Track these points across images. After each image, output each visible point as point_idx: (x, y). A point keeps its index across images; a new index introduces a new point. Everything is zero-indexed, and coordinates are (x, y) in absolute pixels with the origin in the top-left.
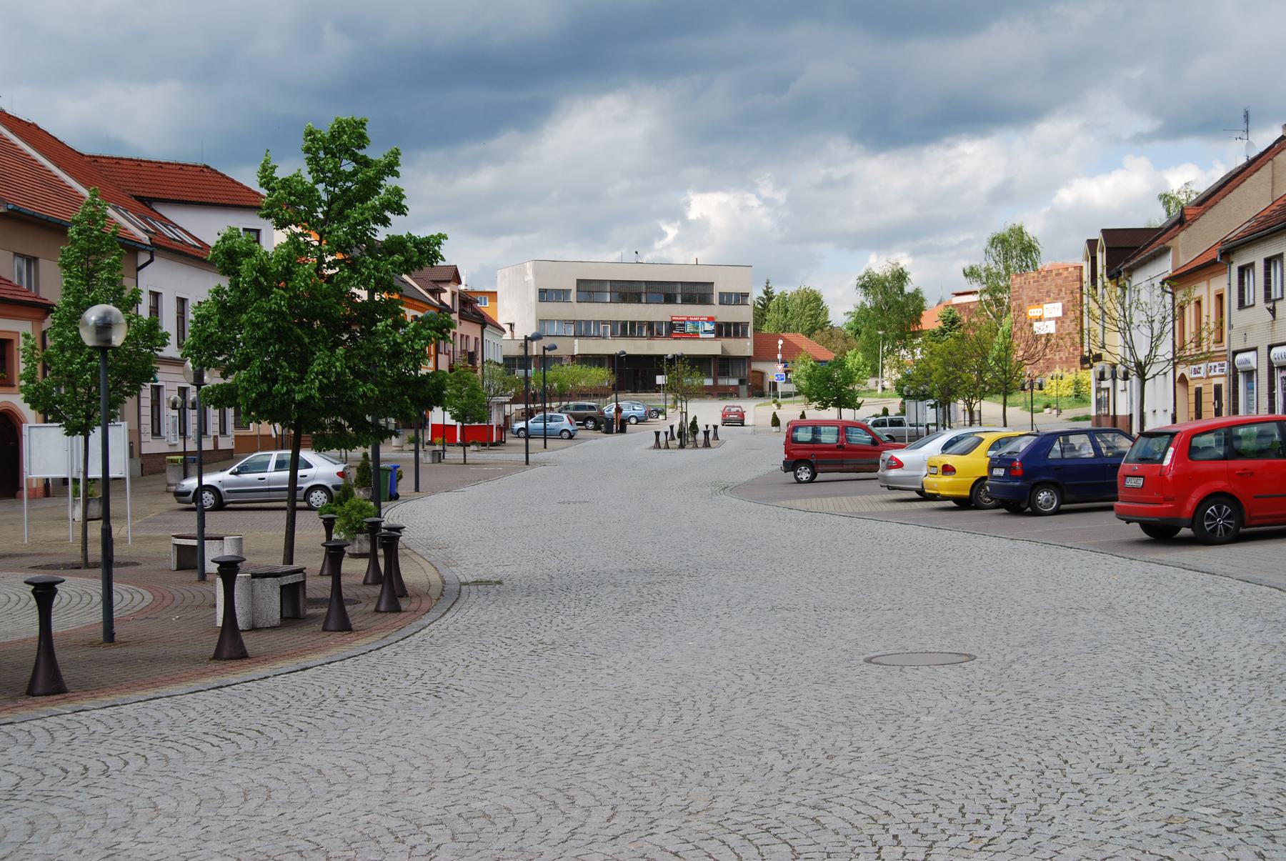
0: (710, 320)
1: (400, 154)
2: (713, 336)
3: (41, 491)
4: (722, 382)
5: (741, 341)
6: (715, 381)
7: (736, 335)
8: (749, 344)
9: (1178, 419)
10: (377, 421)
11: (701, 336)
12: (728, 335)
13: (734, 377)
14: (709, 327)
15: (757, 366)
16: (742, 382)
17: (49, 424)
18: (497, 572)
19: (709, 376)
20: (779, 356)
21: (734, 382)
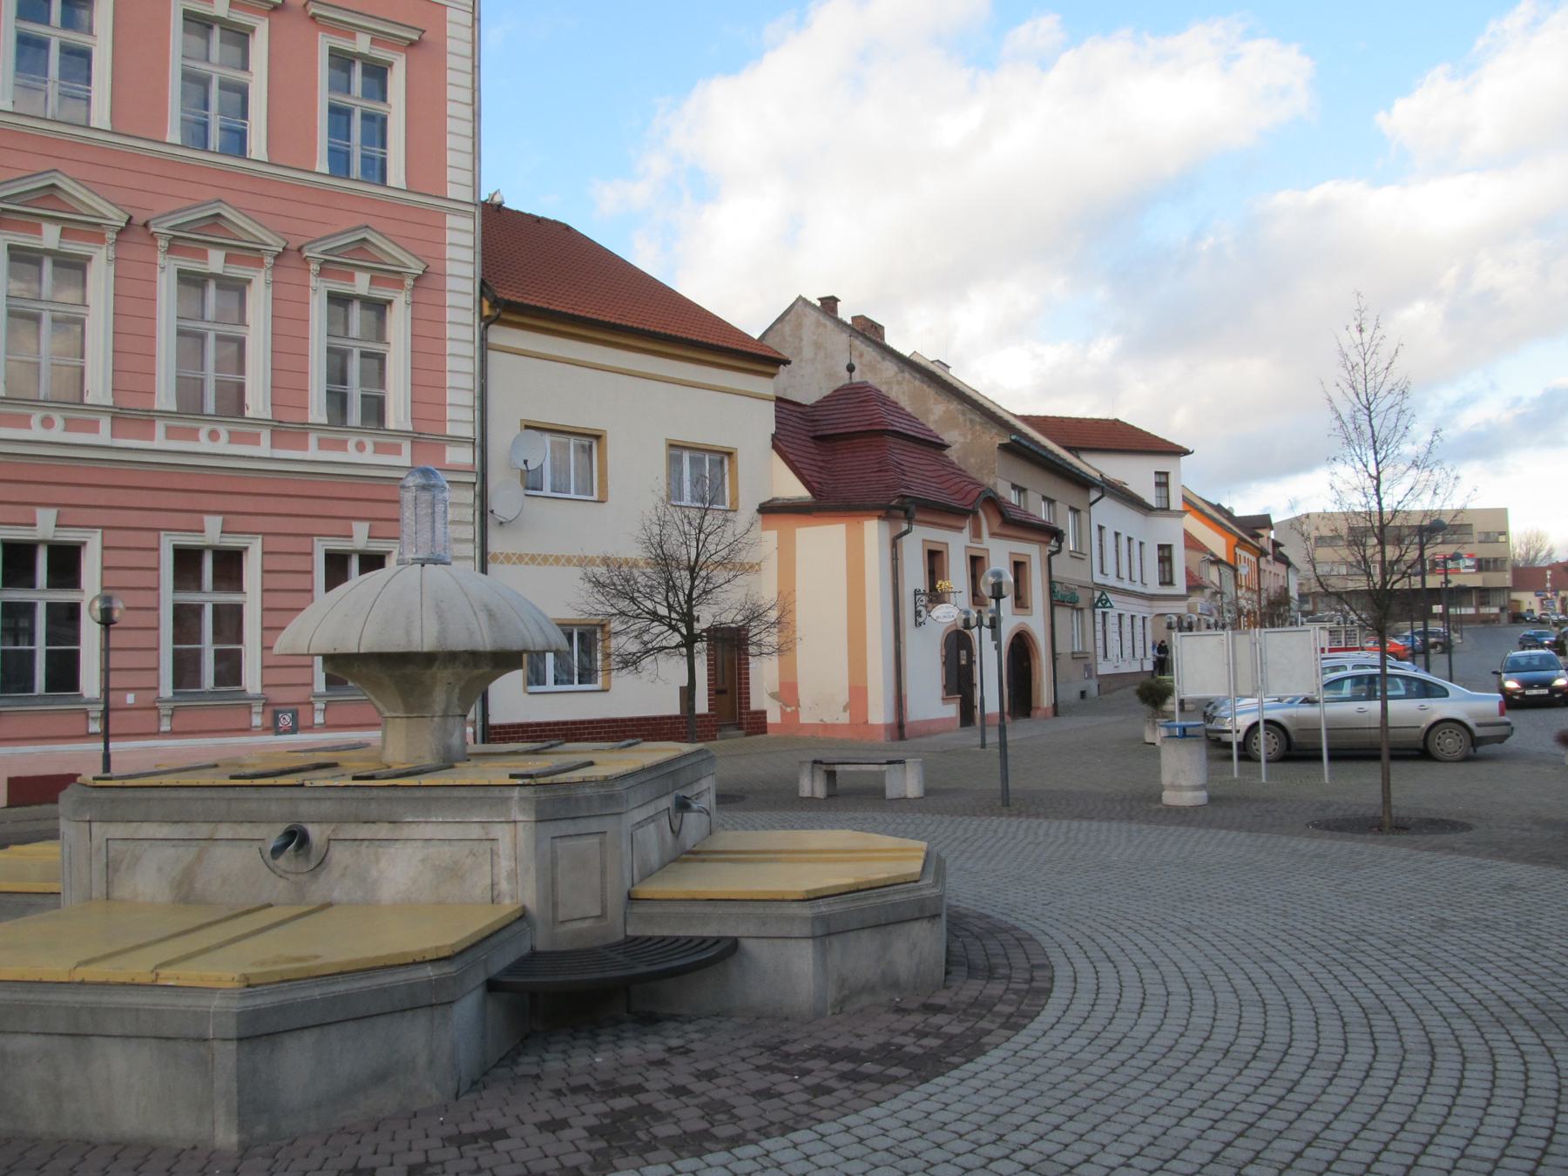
0: (1470, 556)
1: (829, 304)
2: (1474, 570)
3: (1051, 711)
4: (1484, 610)
5: (1499, 575)
6: (1477, 610)
7: (1496, 570)
8: (1507, 576)
9: (1077, 507)
10: (1448, 611)
11: (1462, 571)
12: (1488, 570)
13: (1494, 606)
14: (1469, 563)
15: (1515, 596)
16: (1502, 609)
17: (1277, 629)
18: (945, 948)
19: (1470, 605)
20: (1548, 585)
21: (1495, 610)
